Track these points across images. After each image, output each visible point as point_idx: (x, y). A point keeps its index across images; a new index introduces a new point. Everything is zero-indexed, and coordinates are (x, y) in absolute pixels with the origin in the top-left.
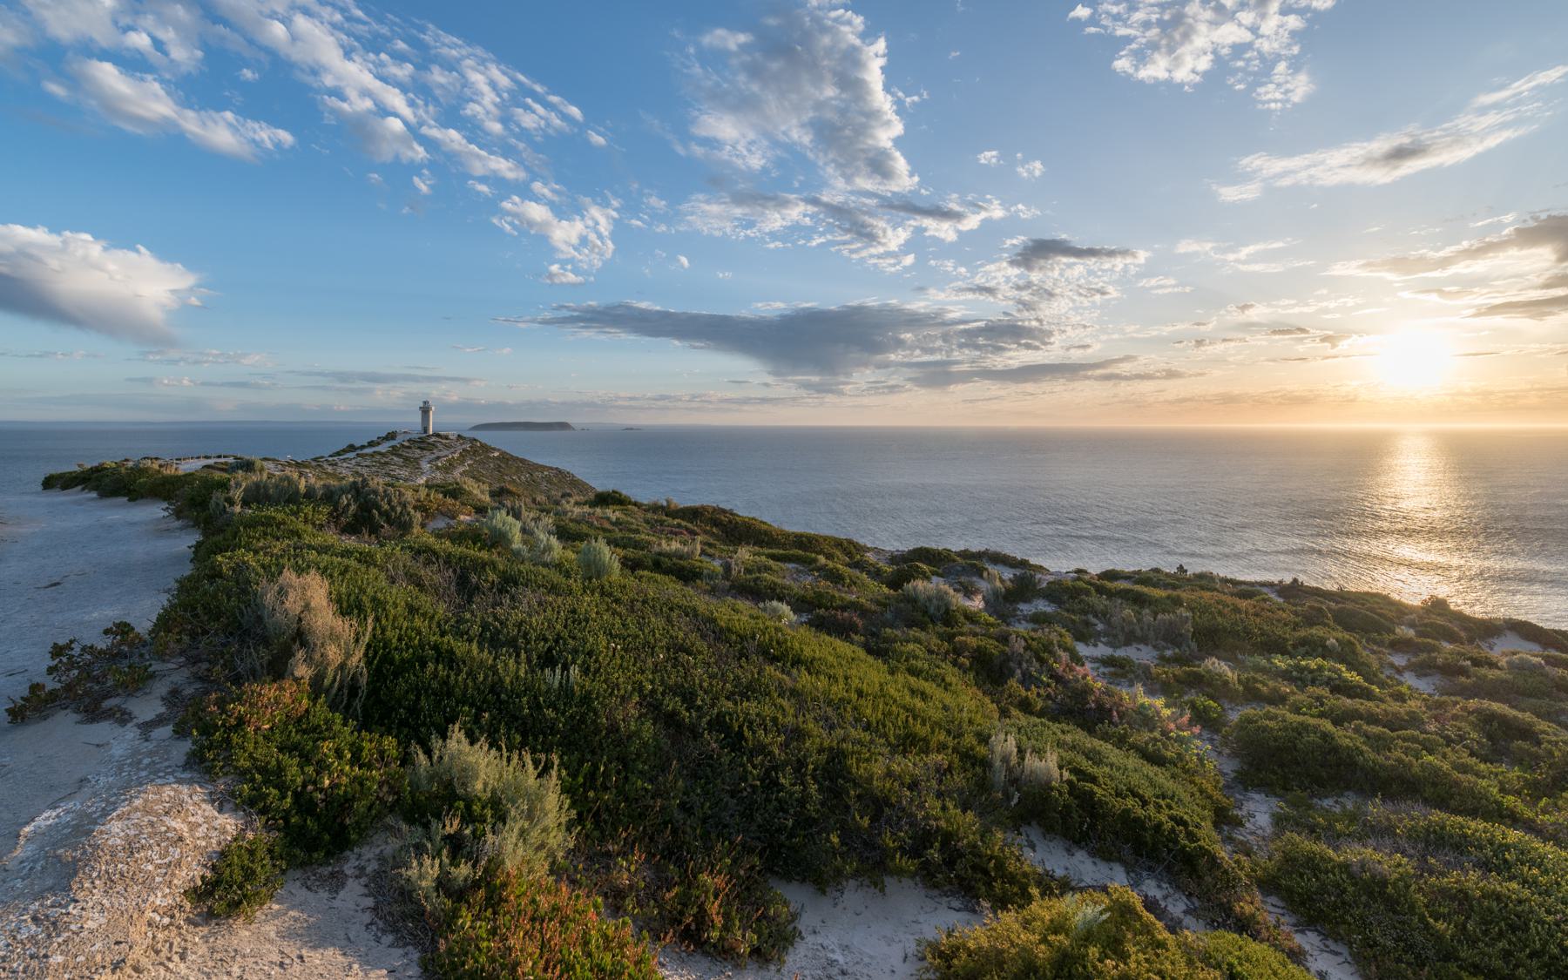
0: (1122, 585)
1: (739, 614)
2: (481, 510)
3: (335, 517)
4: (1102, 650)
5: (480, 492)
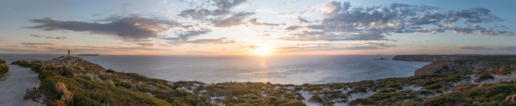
0: (221, 85)
1: (141, 95)
2: (84, 73)
3: (60, 72)
4: (216, 98)
5: (83, 69)
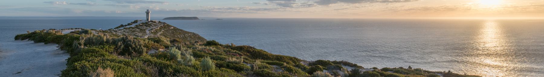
0: (389, 73)
2: (167, 47)
3: (116, 49)
5: (166, 41)
